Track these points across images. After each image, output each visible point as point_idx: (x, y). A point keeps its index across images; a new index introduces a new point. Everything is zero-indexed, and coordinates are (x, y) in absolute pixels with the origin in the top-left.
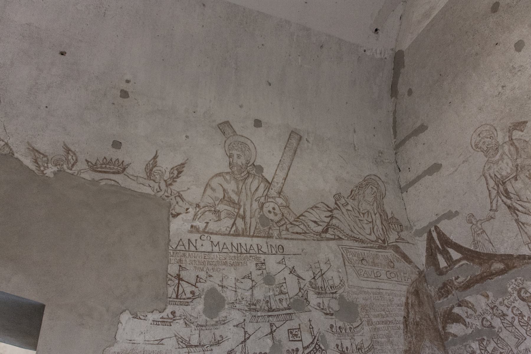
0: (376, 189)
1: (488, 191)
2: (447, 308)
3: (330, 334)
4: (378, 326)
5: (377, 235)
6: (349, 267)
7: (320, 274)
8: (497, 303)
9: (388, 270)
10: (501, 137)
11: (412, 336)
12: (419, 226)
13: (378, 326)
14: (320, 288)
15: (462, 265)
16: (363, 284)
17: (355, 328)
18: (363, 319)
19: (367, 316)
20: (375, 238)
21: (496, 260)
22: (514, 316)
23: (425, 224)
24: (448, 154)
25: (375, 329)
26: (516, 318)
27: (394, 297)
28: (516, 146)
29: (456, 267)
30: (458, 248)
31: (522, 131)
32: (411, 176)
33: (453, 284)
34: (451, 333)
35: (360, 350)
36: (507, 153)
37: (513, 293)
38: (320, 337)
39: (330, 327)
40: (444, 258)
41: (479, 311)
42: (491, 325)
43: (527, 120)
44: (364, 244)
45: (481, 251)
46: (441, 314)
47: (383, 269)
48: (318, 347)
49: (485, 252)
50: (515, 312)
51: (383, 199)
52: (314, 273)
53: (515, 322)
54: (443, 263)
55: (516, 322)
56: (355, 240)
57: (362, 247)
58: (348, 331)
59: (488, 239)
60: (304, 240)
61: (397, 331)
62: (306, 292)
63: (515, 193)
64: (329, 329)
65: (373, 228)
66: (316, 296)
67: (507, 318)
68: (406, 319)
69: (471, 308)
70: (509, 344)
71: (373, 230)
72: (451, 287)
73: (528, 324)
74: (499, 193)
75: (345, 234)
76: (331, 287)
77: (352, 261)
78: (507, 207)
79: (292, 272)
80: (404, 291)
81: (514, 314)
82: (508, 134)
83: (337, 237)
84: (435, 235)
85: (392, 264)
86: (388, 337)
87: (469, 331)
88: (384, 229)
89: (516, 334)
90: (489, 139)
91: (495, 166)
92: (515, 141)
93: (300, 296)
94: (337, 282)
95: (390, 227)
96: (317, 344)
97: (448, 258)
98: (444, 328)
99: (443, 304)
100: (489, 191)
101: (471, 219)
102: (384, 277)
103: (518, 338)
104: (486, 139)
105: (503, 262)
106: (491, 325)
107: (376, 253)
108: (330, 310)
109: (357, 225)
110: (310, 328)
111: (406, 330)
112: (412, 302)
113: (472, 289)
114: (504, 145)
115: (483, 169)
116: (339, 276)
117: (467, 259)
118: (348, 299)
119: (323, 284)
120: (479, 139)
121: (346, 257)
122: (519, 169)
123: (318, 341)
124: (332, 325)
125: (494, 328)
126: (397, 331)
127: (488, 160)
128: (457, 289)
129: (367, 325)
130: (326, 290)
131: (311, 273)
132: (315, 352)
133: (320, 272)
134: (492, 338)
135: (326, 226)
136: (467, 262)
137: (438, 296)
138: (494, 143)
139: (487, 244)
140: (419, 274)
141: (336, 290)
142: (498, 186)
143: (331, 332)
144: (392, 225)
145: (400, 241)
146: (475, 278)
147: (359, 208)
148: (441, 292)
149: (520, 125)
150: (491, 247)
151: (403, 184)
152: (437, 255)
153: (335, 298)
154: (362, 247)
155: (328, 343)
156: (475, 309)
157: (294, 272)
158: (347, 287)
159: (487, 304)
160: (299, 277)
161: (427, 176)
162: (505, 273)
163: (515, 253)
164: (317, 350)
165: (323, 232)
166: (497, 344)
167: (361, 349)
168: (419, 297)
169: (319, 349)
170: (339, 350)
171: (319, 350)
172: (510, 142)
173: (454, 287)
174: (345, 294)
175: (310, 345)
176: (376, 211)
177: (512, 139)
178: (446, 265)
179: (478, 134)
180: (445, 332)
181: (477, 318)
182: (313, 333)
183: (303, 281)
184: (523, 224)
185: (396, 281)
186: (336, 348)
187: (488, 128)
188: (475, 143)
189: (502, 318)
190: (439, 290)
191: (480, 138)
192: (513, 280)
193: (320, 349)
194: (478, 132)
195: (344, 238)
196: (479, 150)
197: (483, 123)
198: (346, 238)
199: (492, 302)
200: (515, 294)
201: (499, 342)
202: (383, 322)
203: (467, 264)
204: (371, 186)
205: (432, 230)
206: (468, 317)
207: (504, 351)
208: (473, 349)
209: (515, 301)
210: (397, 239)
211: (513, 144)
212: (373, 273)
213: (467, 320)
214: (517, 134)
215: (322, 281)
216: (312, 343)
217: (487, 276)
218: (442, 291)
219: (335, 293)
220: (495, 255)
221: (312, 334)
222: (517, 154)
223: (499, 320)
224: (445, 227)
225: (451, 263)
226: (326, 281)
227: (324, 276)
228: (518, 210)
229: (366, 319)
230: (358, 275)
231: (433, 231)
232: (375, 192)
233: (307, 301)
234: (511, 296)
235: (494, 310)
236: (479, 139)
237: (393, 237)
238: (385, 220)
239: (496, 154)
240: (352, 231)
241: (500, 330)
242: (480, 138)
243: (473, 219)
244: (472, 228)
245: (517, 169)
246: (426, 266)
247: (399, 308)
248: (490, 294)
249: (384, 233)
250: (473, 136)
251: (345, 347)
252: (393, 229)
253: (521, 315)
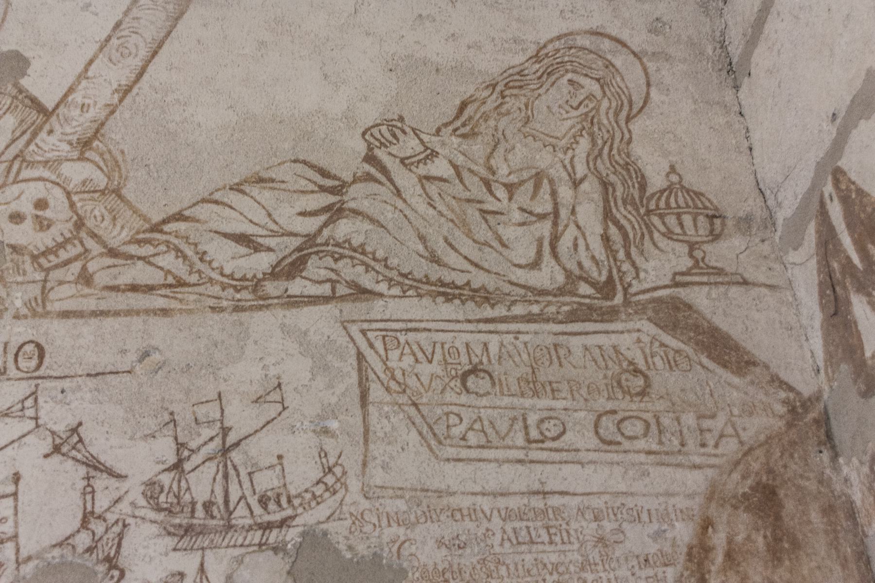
57: (479, 321)
107: (550, 340)
112: (730, 541)
118: (350, 548)
205: (826, 195)
219: (283, 523)
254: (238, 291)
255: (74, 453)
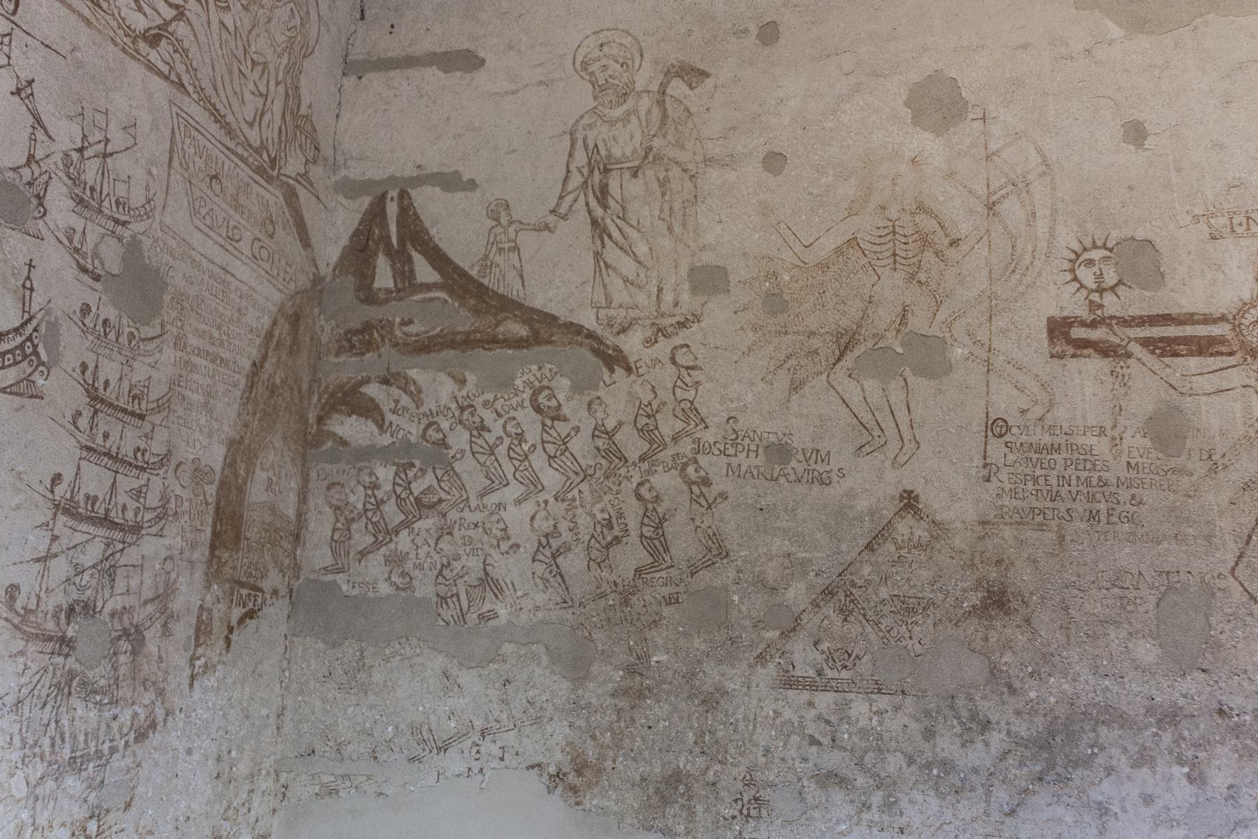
0: (299, 23)
1: (565, 172)
2: (350, 378)
3: (75, 328)
4: (196, 360)
5: (265, 138)
6: (178, 176)
7: (100, 147)
8: (478, 403)
9: (259, 236)
10: (645, 77)
11: (254, 413)
12: (356, 172)
13: (196, 360)
14: (88, 186)
15: (432, 299)
16: (196, 239)
17: (143, 340)
18: (169, 327)
19: (179, 324)
20: (258, 144)
21: (515, 316)
22: (503, 435)
23: (378, 175)
24: (511, 48)
25: (187, 363)
26: (507, 441)
27: (250, 307)
28: (665, 110)
29: (415, 298)
30: (439, 259)
31: (691, 88)
32: (390, 47)
33: (392, 332)
34: (335, 434)
35: (136, 401)
36: (642, 114)
37: (523, 392)
38: (44, 323)
39: (82, 310)
40: (393, 269)
41: (429, 405)
42: (443, 440)
43: (711, 72)
44: (231, 139)
45: (491, 287)
46: (327, 388)
47: (250, 228)
48: (31, 350)
49: (501, 291)
50: (509, 428)
51: (304, 57)
52: (85, 137)
53: (500, 447)
54: (384, 276)
55: (502, 450)
56: (213, 114)
57: (224, 145)
58: (124, 339)
59: (518, 265)
60: (88, 22)
61: (230, 388)
62: (45, 177)
63: (620, 201)
64: (78, 312)
65: (262, 114)
66: (71, 203)
67: (486, 435)
68: (257, 367)
69: (411, 394)
70: (466, 486)
71: (261, 120)
72: (383, 337)
73: (527, 457)
74: (587, 187)
75: (197, 83)
76: (117, 202)
77: (191, 165)
78: (589, 221)
79: (23, 95)
80: (275, 305)
81: (505, 431)
82: (661, 77)
83: (173, 77)
84: (392, 209)
85: (270, 228)
86: (209, 394)
87: (386, 440)
88: (284, 132)
89: (493, 470)
90: (618, 66)
91: (605, 128)
92: (668, 100)
93: (25, 180)
94: (137, 198)
95: (295, 135)
96: (30, 339)
97: (404, 274)
98: (320, 420)
99: (343, 369)
100: (568, 171)
101: (498, 211)
102: (244, 246)
103: (491, 479)
104: (611, 62)
105: (530, 324)
106: (443, 440)
107: (247, 179)
108: (96, 262)
109: (231, 80)
110: (24, 286)
111: (247, 394)
112: (280, 336)
113: (433, 355)
114: (644, 95)
115: (577, 121)
116: (147, 186)
117: (451, 292)
118: (149, 258)
119: (98, 182)
120: (596, 53)
121: (180, 145)
122: (651, 158)
123: (35, 334)
124: (88, 305)
125: (447, 447)
126: (230, 388)
127: (596, 108)
128: (396, 345)
129: (172, 345)
130: (102, 202)
131: (76, 131)
132: (19, 358)
133: (103, 143)
134: (434, 468)
135: (159, 27)
136: (446, 297)
137: (336, 346)
138: (624, 79)
139: (512, 276)
140: (314, 281)
141: (127, 218)
142: (591, 171)
143: (80, 324)
144: (301, 133)
145: (304, 182)
146: (450, 337)
147: (248, 40)
148: (349, 341)
149: (693, 74)
150: (517, 284)
151: (357, 54)
152: (376, 255)
153: (118, 239)
154: (224, 145)
155: (61, 349)
156: (420, 398)
157: (28, 98)
158: (156, 225)
159: (455, 397)
160: (39, 123)
161: (434, 68)
162: (523, 347)
163: (562, 314)
164: (25, 357)
165: (144, 36)
166: (439, 481)
167: (139, 399)
168: (296, 334)
169: (31, 354)
170: (84, 380)
171: (31, 360)
172: (657, 96)
173: (390, 340)
174: (147, 242)
175: (8, 333)
176: (280, 78)
177: (664, 92)
178: (391, 285)
179: (600, 42)
180: (318, 429)
181: (416, 419)
182: (27, 304)
183: (47, 139)
184: (607, 266)
185: (266, 272)
186: (78, 371)
187: (628, 41)
188: (585, 57)
189: (475, 433)
190: (346, 334)
191: (601, 54)
192: (535, 367)
193: (33, 358)
194: (603, 37)
195: (191, 92)
196: (587, 77)
197: (621, 27)
198: (195, 96)
199: (468, 397)
200: (526, 396)
201: (445, 478)
202: (208, 353)
203: (446, 301)
204: (292, 5)
205: (389, 196)
206: (394, 412)
207: (449, 497)
208: (377, 479)
209: (519, 408)
210: (301, 176)
211: (661, 103)
212: (225, 224)
213: (390, 417)
214: (677, 88)
215: (100, 172)
216: (16, 330)
217: (480, 341)
218: (355, 338)
219: (124, 224)
220: (520, 306)
221: (24, 304)
222: (660, 128)
223: (467, 435)
224: (428, 201)
225: (407, 284)
226: (111, 180)
227: (109, 160)
228: (610, 237)
229: (174, 330)
230: (194, 212)
231: (392, 199)
232: (295, 27)
233: (41, 204)
234: (516, 395)
235: (466, 413)
236: (596, 53)
237: (293, 165)
238: (292, 112)
239: (619, 105)
240: (215, 87)
241: (458, 456)
242: (601, 54)
243: (503, 214)
244: (493, 231)
245: (646, 157)
246: (334, 270)
247: (250, 336)
248: (471, 378)
249: (280, 142)
250: (587, 40)
251: (102, 380)
252: (301, 146)
253: (520, 437)
254: (126, 36)
255: (27, 101)
